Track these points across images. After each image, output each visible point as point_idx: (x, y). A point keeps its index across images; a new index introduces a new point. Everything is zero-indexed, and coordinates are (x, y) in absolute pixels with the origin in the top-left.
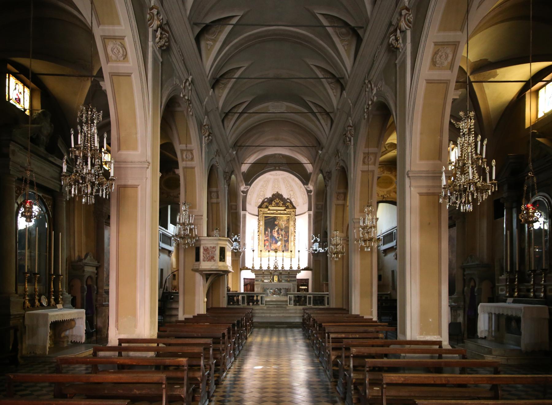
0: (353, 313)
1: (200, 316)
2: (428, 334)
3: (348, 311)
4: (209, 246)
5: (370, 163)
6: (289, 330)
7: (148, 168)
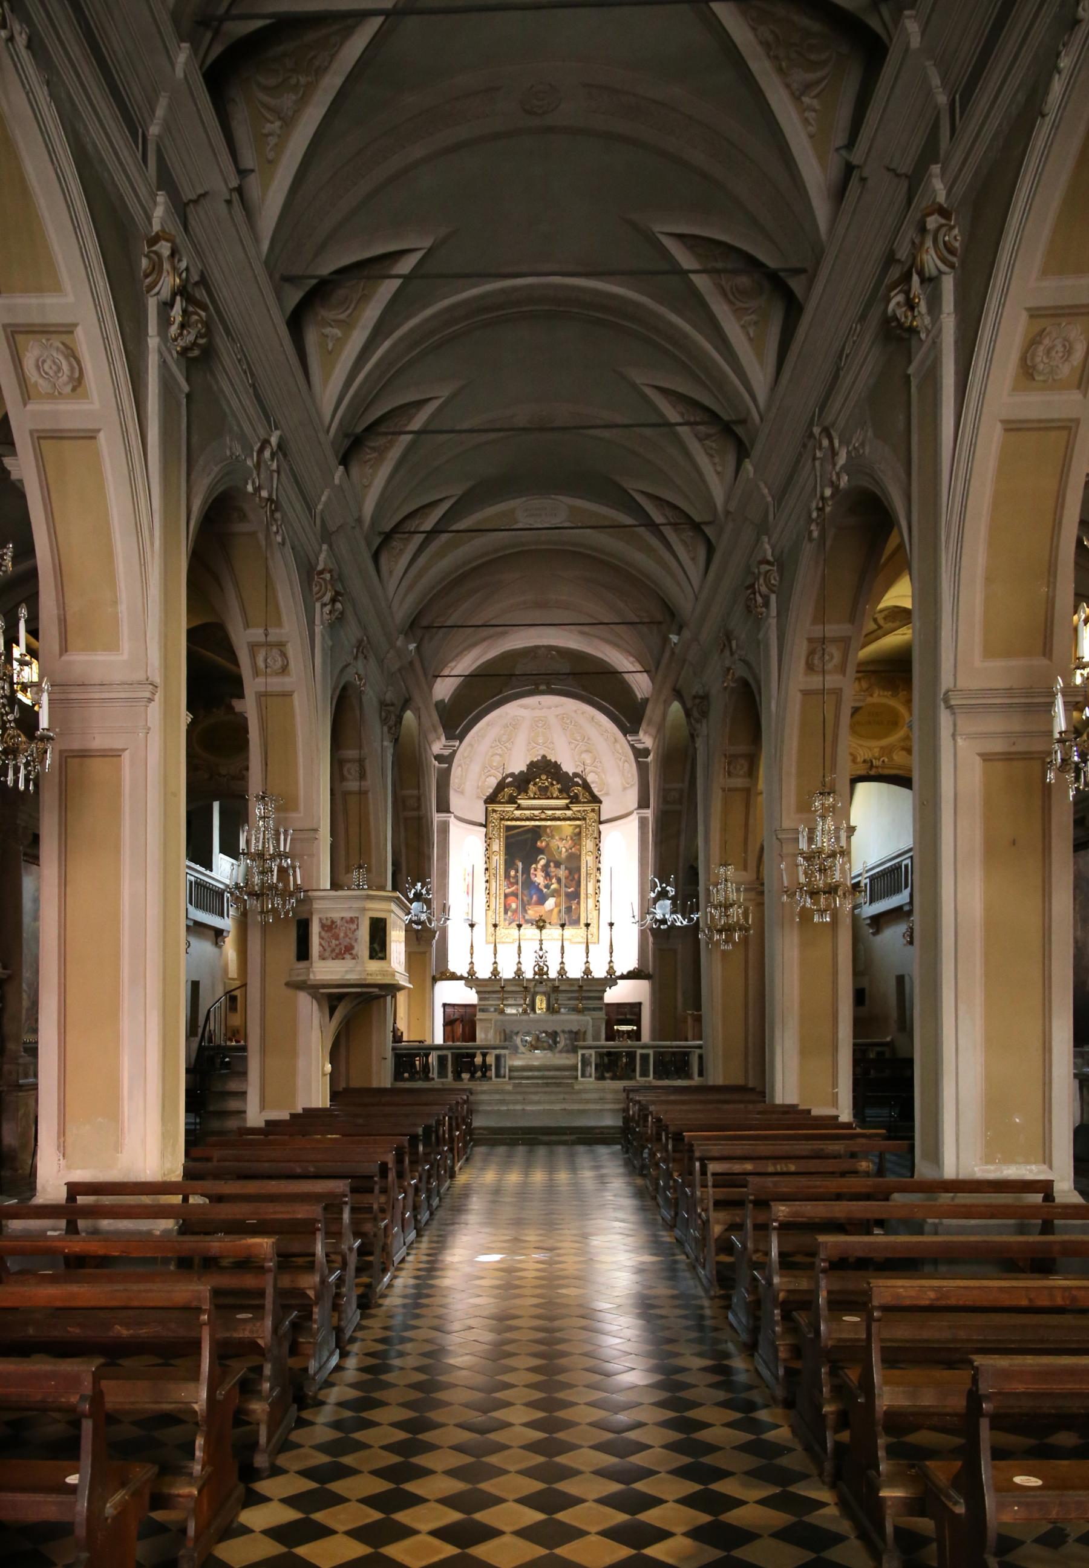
0: (778, 1101)
1: (310, 1114)
2: (1009, 1160)
3: (763, 1094)
4: (336, 916)
5: (829, 666)
6: (581, 1149)
7: (151, 700)
